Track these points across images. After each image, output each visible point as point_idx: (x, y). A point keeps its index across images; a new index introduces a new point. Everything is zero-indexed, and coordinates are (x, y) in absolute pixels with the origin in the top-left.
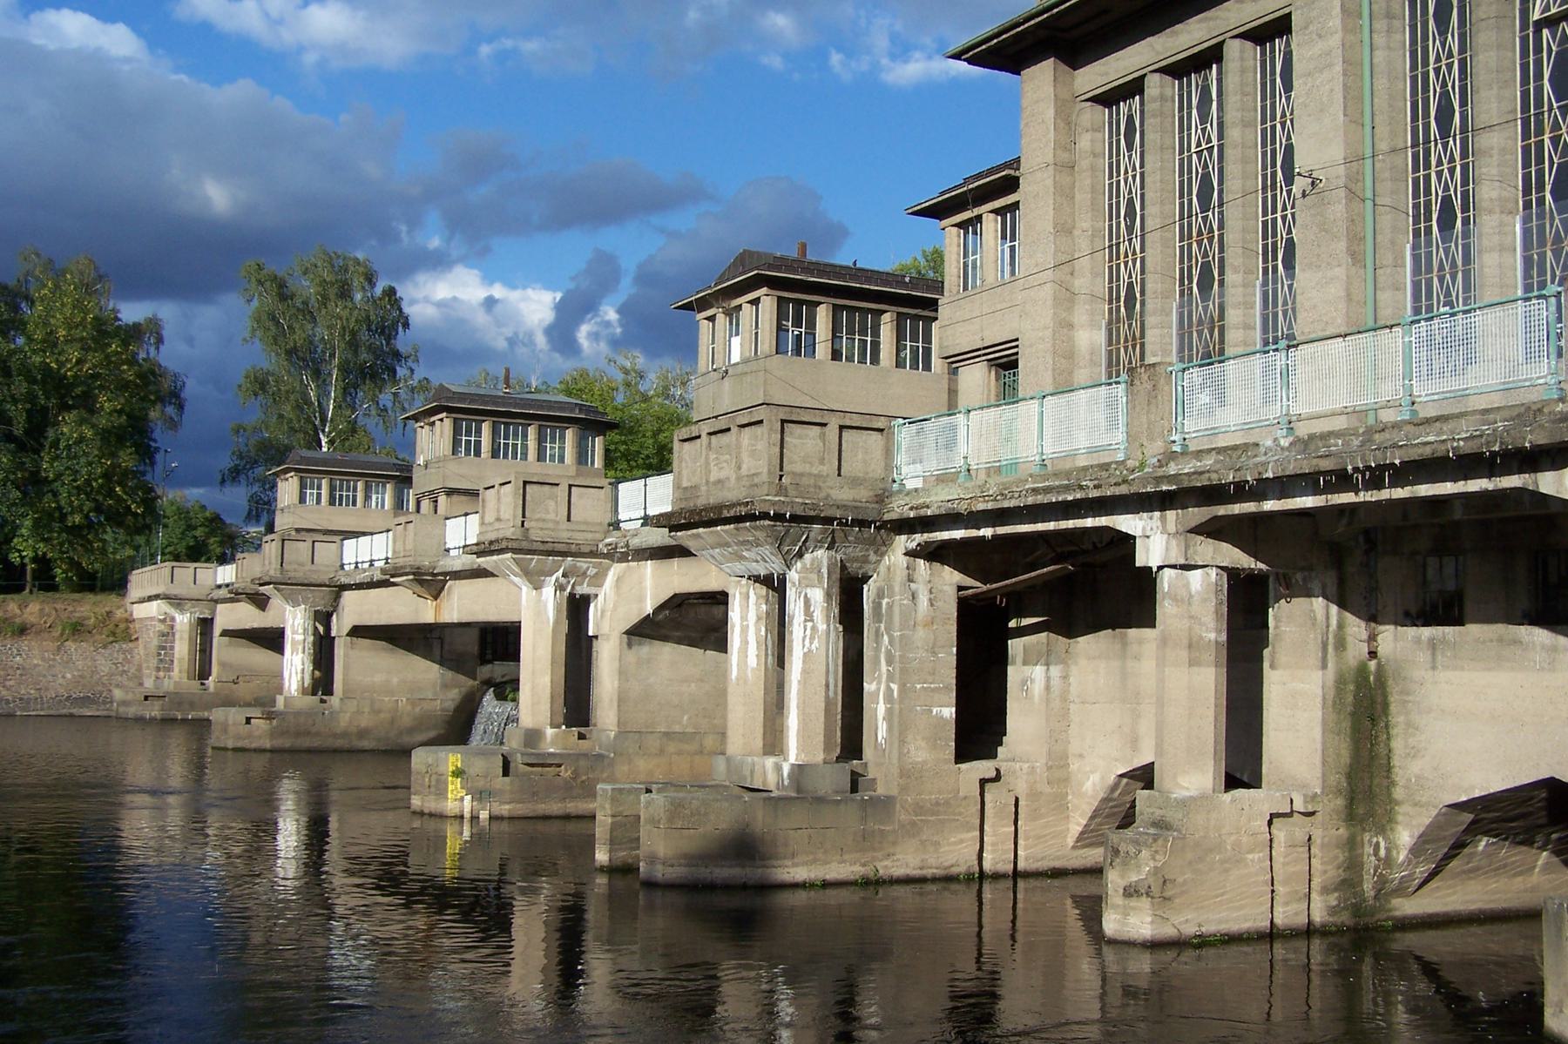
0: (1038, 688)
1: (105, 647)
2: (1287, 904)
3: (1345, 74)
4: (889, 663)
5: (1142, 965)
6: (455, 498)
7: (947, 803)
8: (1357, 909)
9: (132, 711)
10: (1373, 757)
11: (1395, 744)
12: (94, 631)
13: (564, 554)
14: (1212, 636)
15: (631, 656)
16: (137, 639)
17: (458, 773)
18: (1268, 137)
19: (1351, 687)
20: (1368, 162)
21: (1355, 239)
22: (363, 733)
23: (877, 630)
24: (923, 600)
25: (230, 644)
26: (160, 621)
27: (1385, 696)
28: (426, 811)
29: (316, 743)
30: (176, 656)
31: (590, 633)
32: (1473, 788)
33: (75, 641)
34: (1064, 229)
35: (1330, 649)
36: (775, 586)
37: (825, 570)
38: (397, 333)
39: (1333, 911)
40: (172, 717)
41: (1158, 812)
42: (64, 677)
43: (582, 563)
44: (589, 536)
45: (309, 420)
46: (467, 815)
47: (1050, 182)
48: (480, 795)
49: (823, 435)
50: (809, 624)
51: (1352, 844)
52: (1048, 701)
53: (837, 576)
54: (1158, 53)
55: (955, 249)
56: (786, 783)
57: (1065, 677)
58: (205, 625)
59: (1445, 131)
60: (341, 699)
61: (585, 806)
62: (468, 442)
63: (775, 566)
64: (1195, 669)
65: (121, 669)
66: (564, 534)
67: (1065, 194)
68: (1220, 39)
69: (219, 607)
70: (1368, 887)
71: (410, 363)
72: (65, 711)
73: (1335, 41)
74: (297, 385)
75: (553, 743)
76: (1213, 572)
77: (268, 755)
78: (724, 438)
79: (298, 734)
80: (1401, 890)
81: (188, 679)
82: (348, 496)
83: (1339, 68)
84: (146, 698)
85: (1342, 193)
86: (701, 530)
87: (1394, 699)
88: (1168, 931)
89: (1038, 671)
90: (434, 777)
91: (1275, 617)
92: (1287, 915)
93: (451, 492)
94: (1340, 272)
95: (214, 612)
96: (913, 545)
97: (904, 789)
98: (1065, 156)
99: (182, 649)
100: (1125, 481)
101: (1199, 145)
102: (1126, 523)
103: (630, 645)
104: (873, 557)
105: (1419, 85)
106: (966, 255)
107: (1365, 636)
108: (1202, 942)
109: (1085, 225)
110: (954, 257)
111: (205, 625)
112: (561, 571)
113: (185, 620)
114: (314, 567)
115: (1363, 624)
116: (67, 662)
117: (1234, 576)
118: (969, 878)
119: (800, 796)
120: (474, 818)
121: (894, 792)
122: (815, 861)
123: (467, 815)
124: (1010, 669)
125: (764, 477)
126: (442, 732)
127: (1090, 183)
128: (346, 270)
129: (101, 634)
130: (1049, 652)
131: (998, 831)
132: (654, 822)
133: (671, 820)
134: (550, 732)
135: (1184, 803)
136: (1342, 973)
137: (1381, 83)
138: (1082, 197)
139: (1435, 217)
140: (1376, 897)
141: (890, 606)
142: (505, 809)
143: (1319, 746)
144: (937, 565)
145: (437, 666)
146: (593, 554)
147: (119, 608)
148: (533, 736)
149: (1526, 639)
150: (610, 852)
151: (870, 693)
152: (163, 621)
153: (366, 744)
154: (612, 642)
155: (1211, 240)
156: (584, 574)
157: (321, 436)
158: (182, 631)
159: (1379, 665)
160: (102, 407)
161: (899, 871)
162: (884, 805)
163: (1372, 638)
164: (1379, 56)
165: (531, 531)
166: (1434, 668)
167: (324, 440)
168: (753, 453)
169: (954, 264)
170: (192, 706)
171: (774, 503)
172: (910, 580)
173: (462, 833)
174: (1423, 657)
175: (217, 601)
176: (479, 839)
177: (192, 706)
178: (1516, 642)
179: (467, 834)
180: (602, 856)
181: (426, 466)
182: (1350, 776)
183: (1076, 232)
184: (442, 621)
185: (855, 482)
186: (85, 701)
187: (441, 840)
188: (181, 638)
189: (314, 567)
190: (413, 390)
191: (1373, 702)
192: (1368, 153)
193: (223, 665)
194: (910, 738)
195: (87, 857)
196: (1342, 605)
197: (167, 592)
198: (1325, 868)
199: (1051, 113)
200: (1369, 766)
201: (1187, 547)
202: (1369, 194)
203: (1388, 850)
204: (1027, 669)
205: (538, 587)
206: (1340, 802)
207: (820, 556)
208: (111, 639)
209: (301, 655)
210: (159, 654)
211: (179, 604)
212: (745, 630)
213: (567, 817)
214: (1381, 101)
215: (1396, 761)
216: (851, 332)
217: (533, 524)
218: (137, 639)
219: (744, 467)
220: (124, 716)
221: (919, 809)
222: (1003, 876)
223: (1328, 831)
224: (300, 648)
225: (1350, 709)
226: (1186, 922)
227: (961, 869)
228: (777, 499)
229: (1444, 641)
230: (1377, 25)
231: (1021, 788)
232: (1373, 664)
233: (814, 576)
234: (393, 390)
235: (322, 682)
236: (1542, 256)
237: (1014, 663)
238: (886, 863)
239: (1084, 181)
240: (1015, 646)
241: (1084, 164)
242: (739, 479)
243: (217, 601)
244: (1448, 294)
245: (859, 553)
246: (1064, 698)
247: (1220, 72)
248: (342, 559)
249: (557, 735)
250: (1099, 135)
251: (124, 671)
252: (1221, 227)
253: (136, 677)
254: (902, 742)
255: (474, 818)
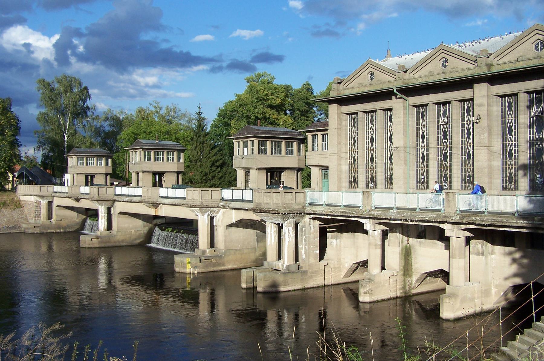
0: (334, 244)
1: (14, 210)
2: (393, 293)
3: (404, 127)
4: (305, 241)
5: (368, 306)
6: (145, 173)
7: (318, 271)
8: (405, 293)
9: (30, 231)
10: (408, 263)
11: (412, 261)
12: (10, 205)
13: (211, 208)
14: (379, 243)
15: (227, 231)
16: (23, 207)
17: (189, 263)
18: (386, 132)
19: (404, 250)
20: (408, 148)
21: (405, 161)
22: (123, 241)
23: (302, 235)
24: (312, 228)
25: (59, 209)
26: (35, 202)
27: (411, 251)
28: (180, 272)
29: (110, 245)
30: (42, 213)
31: (214, 225)
32: (427, 270)
33: (5, 208)
34: (339, 143)
35: (400, 243)
36: (280, 227)
37: (292, 223)
38: (87, 100)
39: (401, 293)
40: (42, 232)
41: (369, 277)
42: (4, 220)
43: (215, 209)
44: (216, 203)
45: (61, 130)
46: (192, 273)
47: (336, 133)
48: (194, 267)
49: (292, 195)
50: (289, 235)
51: (404, 281)
52: (337, 247)
53: (294, 224)
54: (361, 108)
55: (310, 140)
56: (285, 269)
57: (340, 242)
58: (50, 204)
59: (423, 140)
60: (117, 232)
61: (217, 268)
62: (148, 157)
63: (281, 222)
64: (376, 250)
65: (21, 217)
66: (210, 202)
67: (339, 135)
68: (376, 109)
69: (55, 198)
70: (407, 288)
71: (92, 111)
72: (8, 232)
73: (402, 119)
74: (56, 118)
75: (208, 253)
76: (379, 231)
77: (98, 249)
78: (269, 194)
79: (106, 242)
80: (413, 288)
81: (46, 220)
82: (92, 162)
83: (402, 125)
84: (35, 227)
85: (403, 151)
86: (263, 213)
87: (412, 252)
88: (372, 300)
89: (335, 241)
90: (182, 264)
91: (389, 236)
92: (393, 295)
93: (144, 172)
94: (402, 167)
95: (53, 199)
96: (311, 217)
97: (309, 269)
98: (339, 126)
99: (44, 211)
100: (363, 214)
101: (371, 129)
102: (361, 220)
103: (227, 229)
104: (301, 219)
105: (418, 129)
106: (313, 142)
107: (407, 239)
108: (378, 301)
109: (344, 142)
110: (310, 142)
111: (50, 204)
112: (209, 211)
113: (44, 202)
114: (107, 195)
115: (406, 238)
116: (4, 215)
117: (383, 231)
118: (322, 287)
119: (289, 272)
120: (193, 273)
121: (307, 269)
122: (292, 286)
123: (192, 273)
124: (327, 240)
125: (281, 205)
126: (144, 239)
127: (345, 133)
128: (71, 82)
129: (12, 205)
130: (337, 237)
131: (328, 277)
132: (260, 279)
133: (264, 278)
134: (208, 250)
135: (374, 275)
136: (402, 305)
137: (411, 128)
138: (343, 136)
139: (421, 157)
140: (409, 290)
141: (305, 230)
142: (201, 270)
143: (398, 262)
144: (315, 220)
145: (142, 221)
146: (218, 207)
147: (15, 196)
148: (204, 252)
149: (437, 243)
150: (246, 285)
151: (300, 248)
152: (36, 202)
153: (124, 244)
154: (222, 228)
155: (373, 151)
156: (215, 211)
157: (65, 134)
158: (43, 206)
159: (409, 245)
160: (7, 134)
161: (309, 286)
162: (305, 272)
163: (408, 240)
164: (410, 123)
165: (203, 203)
166: (420, 247)
167: (66, 136)
168: (277, 199)
169: (310, 144)
170: (49, 228)
171: (284, 211)
172: (310, 224)
173: (190, 277)
174: (418, 244)
175: (54, 197)
176: (195, 278)
177: (49, 228)
178: (435, 243)
179: (192, 277)
180: (244, 286)
181: (135, 164)
182: (404, 267)
183: (342, 144)
184: (158, 215)
185: (299, 204)
186: (13, 228)
187: (185, 279)
188: (43, 208)
189: (107, 195)
190: (94, 119)
191: (408, 252)
192: (408, 146)
193: (57, 215)
194: (310, 257)
195: (137, 289)
196: (402, 235)
197: (39, 194)
198: (399, 285)
199: (336, 117)
200: (407, 265)
201: (375, 227)
202: (408, 151)
203: (411, 281)
204: (332, 240)
205: (203, 215)
206: (402, 272)
207: (291, 220)
208: (15, 207)
209: (104, 220)
210: (36, 213)
211: (43, 198)
212: (271, 234)
213: (214, 271)
214: (410, 132)
215: (412, 264)
216: (275, 147)
217: (203, 201)
218: (23, 207)
219: (274, 201)
220: (27, 232)
221: (312, 273)
222: (329, 285)
223: (400, 278)
224: (104, 218)
225: (404, 254)
226: (375, 298)
227: (320, 285)
228: (284, 210)
229: (422, 242)
230: (410, 116)
231: (332, 266)
232: (408, 245)
233: (290, 225)
234: (87, 119)
235: (109, 227)
236: (441, 169)
237: (328, 238)
238: (306, 285)
239: (344, 132)
240: (329, 235)
241: (344, 128)
242: (273, 204)
243: (54, 197)
244: (423, 173)
245: (298, 218)
246: (340, 246)
247: (375, 115)
248: (115, 192)
249: (209, 251)
250: (347, 122)
251: (22, 217)
252: (375, 149)
253: (26, 219)
254: (309, 259)
255: (193, 273)
